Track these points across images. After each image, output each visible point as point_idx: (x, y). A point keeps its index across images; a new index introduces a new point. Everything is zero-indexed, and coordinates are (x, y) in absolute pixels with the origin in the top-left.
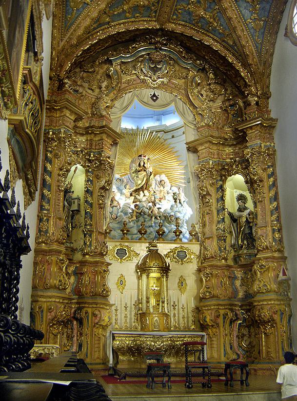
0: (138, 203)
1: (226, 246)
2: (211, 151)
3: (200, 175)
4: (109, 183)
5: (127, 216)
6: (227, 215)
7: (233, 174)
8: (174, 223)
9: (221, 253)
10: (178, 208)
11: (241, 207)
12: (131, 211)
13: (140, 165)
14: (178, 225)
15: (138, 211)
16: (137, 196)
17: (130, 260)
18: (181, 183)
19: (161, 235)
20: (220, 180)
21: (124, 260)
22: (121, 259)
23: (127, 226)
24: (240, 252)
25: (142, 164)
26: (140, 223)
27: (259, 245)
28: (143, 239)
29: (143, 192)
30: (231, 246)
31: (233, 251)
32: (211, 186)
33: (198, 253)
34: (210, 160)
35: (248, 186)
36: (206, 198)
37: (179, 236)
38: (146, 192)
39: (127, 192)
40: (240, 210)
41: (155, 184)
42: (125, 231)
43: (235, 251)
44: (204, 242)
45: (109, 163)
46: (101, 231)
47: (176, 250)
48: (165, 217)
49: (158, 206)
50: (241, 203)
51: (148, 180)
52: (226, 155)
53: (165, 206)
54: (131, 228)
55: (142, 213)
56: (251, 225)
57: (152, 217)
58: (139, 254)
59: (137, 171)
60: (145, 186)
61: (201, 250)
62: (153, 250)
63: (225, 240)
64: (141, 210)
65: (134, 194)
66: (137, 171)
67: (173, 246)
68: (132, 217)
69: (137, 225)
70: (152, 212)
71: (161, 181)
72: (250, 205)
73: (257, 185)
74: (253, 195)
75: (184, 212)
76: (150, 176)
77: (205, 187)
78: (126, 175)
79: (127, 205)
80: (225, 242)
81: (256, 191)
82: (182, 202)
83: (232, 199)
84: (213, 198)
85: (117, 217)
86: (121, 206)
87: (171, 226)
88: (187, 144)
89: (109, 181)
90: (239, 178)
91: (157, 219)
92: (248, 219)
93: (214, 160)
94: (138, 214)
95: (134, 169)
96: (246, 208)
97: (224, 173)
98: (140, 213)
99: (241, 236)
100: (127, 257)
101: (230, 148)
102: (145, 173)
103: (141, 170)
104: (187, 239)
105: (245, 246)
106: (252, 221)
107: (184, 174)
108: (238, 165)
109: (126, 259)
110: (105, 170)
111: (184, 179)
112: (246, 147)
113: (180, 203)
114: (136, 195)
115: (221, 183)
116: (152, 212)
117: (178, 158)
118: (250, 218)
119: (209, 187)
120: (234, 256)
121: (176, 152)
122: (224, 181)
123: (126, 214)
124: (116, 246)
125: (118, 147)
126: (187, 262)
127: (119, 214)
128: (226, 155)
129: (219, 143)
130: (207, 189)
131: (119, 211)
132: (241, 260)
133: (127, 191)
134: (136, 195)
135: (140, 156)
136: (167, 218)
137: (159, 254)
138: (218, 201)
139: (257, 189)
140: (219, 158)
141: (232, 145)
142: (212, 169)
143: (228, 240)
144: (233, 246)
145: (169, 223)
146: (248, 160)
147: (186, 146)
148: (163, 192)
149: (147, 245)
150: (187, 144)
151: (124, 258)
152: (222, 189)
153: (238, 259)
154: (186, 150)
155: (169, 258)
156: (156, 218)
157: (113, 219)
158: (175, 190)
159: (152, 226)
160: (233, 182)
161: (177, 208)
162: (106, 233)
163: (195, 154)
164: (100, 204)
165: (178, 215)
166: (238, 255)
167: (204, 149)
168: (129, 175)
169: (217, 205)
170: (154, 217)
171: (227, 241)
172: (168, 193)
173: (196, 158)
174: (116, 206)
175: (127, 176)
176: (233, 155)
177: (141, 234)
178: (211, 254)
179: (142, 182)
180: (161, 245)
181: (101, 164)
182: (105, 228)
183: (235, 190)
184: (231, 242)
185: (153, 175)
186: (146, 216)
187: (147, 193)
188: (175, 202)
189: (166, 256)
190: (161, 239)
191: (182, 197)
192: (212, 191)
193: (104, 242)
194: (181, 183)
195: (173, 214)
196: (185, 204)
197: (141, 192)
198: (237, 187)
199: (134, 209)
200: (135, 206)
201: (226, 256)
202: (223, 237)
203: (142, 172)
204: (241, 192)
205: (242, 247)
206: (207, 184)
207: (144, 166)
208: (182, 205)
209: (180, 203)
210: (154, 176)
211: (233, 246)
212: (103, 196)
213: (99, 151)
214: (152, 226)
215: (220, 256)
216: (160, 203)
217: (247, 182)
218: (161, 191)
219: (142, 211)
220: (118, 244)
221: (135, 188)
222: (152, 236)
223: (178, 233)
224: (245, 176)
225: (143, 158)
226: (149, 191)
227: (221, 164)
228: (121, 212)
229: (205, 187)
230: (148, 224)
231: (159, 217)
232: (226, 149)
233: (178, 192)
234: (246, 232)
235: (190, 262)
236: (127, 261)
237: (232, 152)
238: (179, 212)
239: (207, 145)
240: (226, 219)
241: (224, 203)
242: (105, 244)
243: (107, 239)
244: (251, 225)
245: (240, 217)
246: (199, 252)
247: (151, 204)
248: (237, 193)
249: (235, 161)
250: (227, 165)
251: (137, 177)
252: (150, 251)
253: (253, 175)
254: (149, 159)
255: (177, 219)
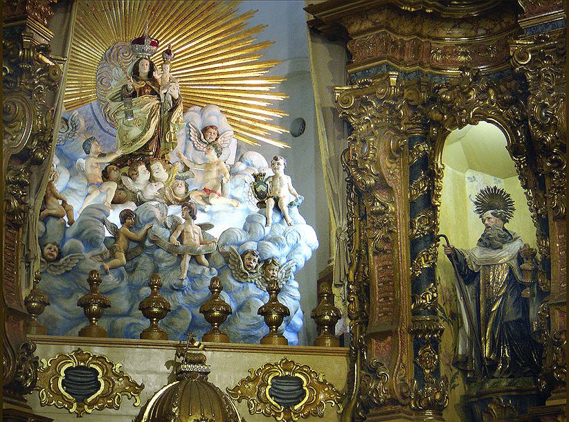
0: (132, 206)
1: (438, 363)
2: (393, 36)
3: (353, 120)
4: (44, 139)
5: (97, 252)
6: (442, 256)
7: (468, 122)
8: (257, 277)
9: (421, 386)
10: (270, 225)
11: (493, 234)
12: (108, 234)
13: (136, 72)
14: (275, 290)
15: (132, 234)
16: (128, 182)
17: (111, 406)
18: (271, 135)
19: (215, 320)
20: (423, 139)
21: (90, 405)
22: (81, 401)
23: (101, 289)
24: (487, 386)
25: (144, 69)
26: (142, 275)
27: (555, 363)
28: (156, 334)
29: (148, 168)
30: (456, 364)
31: (459, 381)
32: (392, 157)
33: (341, 386)
34: (389, 68)
35: (518, 164)
36: (374, 199)
37: (278, 323)
38: (157, 166)
39: (91, 165)
40: (487, 242)
41: (184, 137)
42: (95, 307)
43: (468, 381)
44: (361, 346)
45: (46, 68)
46: (14, 305)
47: (269, 372)
48: (226, 256)
49: (201, 218)
50: (493, 219)
51: (163, 126)
52: (444, 54)
53: (226, 216)
54: (110, 292)
55: (147, 243)
56: (526, 293)
57: (180, 257)
58: (142, 387)
59: (127, 95)
60: (153, 147)
61: (351, 375)
62: (192, 374)
63: (435, 344)
64: (142, 232)
65: (114, 174)
66: (127, 95)
67: (259, 360)
68: (113, 256)
69: (130, 285)
70: (181, 238)
71: (205, 130)
72: (522, 225)
73: (552, 162)
74: (536, 196)
75: (292, 241)
76: (172, 110)
77: (372, 161)
78: (83, 102)
79: (96, 213)
80: (436, 348)
81: (547, 181)
82: (284, 204)
83: (459, 203)
84: (396, 199)
85: (60, 255)
86: (76, 217)
87: (245, 289)
88: (310, 9)
89: (44, 134)
90: (488, 134)
91: (200, 264)
92: (516, 272)
93: (402, 68)
94: (133, 245)
95: (115, 87)
96: (508, 237)
97: (436, 116)
98: (140, 243)
99: (492, 332)
100: (102, 396)
101: (456, 32)
102: (154, 102)
103: (141, 92)
104: (298, 333)
105: (504, 363)
106: (529, 280)
107: (280, 106)
108: (485, 91)
109: (95, 402)
110: (30, 93)
111: (281, 122)
112: (519, 33)
113: (277, 208)
114: (124, 178)
115: (423, 147)
116: (181, 238)
117: (263, 52)
118: (521, 271)
119: (385, 162)
120: (466, 397)
121: (259, 28)
122: (437, 143)
123: (91, 243)
124: (64, 357)
125: (74, 13)
126: (306, 417)
127: (67, 245)
128: (444, 54)
129: (423, 12)
130: (378, 167)
131: (70, 233)
132: (488, 412)
133: (94, 160)
134: (124, 178)
135: (140, 41)
136: (234, 261)
137: (212, 387)
138: (413, 209)
139: (552, 175)
140: (421, 64)
141: (467, 20)
142: (395, 99)
143: (446, 341)
144: (460, 363)
145: (242, 276)
146: (521, 76)
147: (306, 17)
148: (215, 169)
149: (171, 354)
150: (310, 9)
151: (89, 400)
152: (427, 170)
153: (477, 409)
154: (305, 31)
155: (244, 401)
156: (195, 259)
157: (48, 261)
158: (259, 161)
159: (180, 289)
160: (462, 144)
161: (268, 229)
162: (31, 310)
163: (336, 47)
164: (12, 213)
165: (272, 251)
166: (479, 395)
167: (369, 30)
168: (94, 103)
169: (412, 227)
170: (188, 258)
171: (442, 344)
172: (233, 173)
173: (341, 59)
174: (58, 217)
175: (87, 107)
176: (465, 54)
177: (147, 314)
178: (391, 391)
179: (145, 132)
180: (217, 354)
181: (18, 72)
182: (25, 293)
183: (469, 174)
184: (456, 349)
185: (180, 108)
186: (160, 253)
187: (163, 171)
188: (262, 205)
189: (234, 392)
190: (217, 337)
191: (286, 190)
192: (394, 172)
193: (26, 346)
194: (271, 135)
195: (252, 246)
196: (294, 215)
197: (142, 168)
198: (475, 161)
199: (120, 226)
200: (125, 216)
201: (438, 397)
202: (428, 331)
203: (146, 98)
204: (492, 182)
205: (493, 366)
206: (381, 150)
207: (150, 75)
208: (283, 217)
209: (277, 208)
210: (185, 112)
211: (460, 363)
212: (22, 185)
213: (12, 28)
214: (180, 289)
215: (419, 398)
216: (208, 208)
217: (514, 150)
218: (208, 165)
219: (146, 235)
220: (69, 349)
221: (119, 153)
222: (182, 323)
223: (274, 315)
224: (509, 127)
225: (147, 47)
226: (167, 163)
227: (428, 86)
228: (77, 236)
229: (372, 161)
230: (168, 279)
231: (207, 256)
232: (442, 33)
233: (269, 173)
234: (506, 320)
235: (315, 414)
236: (101, 408)
237: (463, 45)
238: (275, 240)
239: (380, 18)
240: (439, 273)
241: (435, 217)
242: (30, 352)
243: (32, 335)
244: (526, 293)
245: (489, 265)
246: (344, 382)
247: (175, 210)
248: (476, 184)
249: (476, 78)
250: (450, 88)
251: (129, 114)
252: (178, 375)
253: (542, 127)
254: (168, 52)
255: (267, 263)
